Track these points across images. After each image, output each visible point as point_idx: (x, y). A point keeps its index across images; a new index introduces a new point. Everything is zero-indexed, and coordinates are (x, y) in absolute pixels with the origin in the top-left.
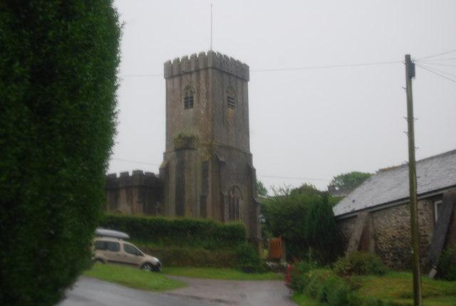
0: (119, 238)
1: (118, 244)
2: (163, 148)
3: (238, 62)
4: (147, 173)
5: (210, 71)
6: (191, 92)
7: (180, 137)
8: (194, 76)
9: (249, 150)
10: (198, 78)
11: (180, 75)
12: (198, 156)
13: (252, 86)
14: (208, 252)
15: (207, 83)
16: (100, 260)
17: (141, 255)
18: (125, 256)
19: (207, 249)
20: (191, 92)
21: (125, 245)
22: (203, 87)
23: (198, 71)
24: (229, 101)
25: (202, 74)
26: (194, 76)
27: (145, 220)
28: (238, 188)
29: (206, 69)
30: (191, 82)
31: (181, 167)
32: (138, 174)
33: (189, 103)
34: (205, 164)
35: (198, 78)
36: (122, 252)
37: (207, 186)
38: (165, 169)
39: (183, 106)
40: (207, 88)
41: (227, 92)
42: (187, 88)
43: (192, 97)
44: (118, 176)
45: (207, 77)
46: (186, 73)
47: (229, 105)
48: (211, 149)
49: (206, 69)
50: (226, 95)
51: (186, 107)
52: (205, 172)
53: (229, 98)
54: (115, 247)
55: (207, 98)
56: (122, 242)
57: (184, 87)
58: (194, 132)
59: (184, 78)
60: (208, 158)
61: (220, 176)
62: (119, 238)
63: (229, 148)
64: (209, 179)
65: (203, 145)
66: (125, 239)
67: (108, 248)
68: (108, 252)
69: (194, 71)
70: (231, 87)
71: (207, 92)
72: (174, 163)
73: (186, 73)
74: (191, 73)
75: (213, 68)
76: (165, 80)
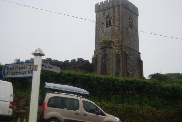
0: (78, 94)
1: (78, 100)
2: (93, 48)
3: (134, 6)
4: (86, 60)
5: (121, 7)
6: (110, 18)
7: (104, 41)
8: (111, 9)
9: (139, 51)
10: (114, 11)
11: (104, 10)
12: (113, 53)
13: (140, 18)
14: (155, 109)
15: (119, 13)
16: (108, 11)
17: (104, 115)
18: (85, 115)
19: (153, 106)
20: (110, 18)
21: (84, 102)
22: (117, 15)
23: (113, 7)
24: (130, 24)
25: (116, 8)
26: (111, 9)
27: (100, 79)
28: (135, 71)
29: (119, 6)
30: (110, 13)
31: (105, 57)
32: (80, 60)
33: (108, 24)
34: (118, 56)
35: (114, 11)
36: (81, 110)
37: (120, 68)
38: (95, 59)
39: (105, 26)
40: (119, 16)
41: (129, 19)
42: (107, 17)
43: (111, 21)
44: (70, 62)
45: (119, 9)
46: (108, 8)
47: (130, 26)
48: (121, 47)
49: (119, 6)
50: (128, 21)
51: (107, 26)
52: (118, 61)
53: (130, 22)
54: (73, 105)
55: (119, 20)
56: (81, 99)
57: (106, 16)
58: (113, 39)
59: (106, 11)
60: (120, 52)
61: (127, 63)
62: (78, 94)
63: (130, 49)
64: (121, 64)
65: (117, 46)
66: (83, 96)
67: (66, 107)
68: (65, 110)
69: (111, 8)
70: (130, 17)
71: (119, 17)
72: (100, 57)
73: (108, 8)
74: (110, 8)
75: (122, 5)
76: (95, 13)
